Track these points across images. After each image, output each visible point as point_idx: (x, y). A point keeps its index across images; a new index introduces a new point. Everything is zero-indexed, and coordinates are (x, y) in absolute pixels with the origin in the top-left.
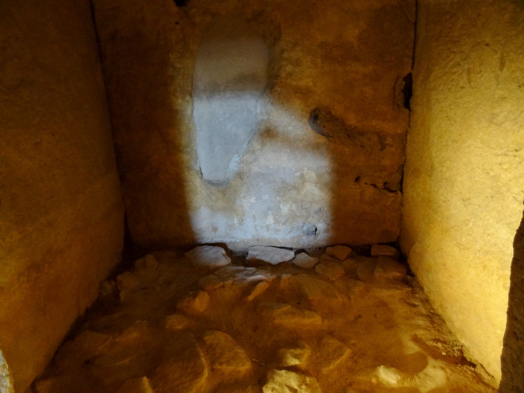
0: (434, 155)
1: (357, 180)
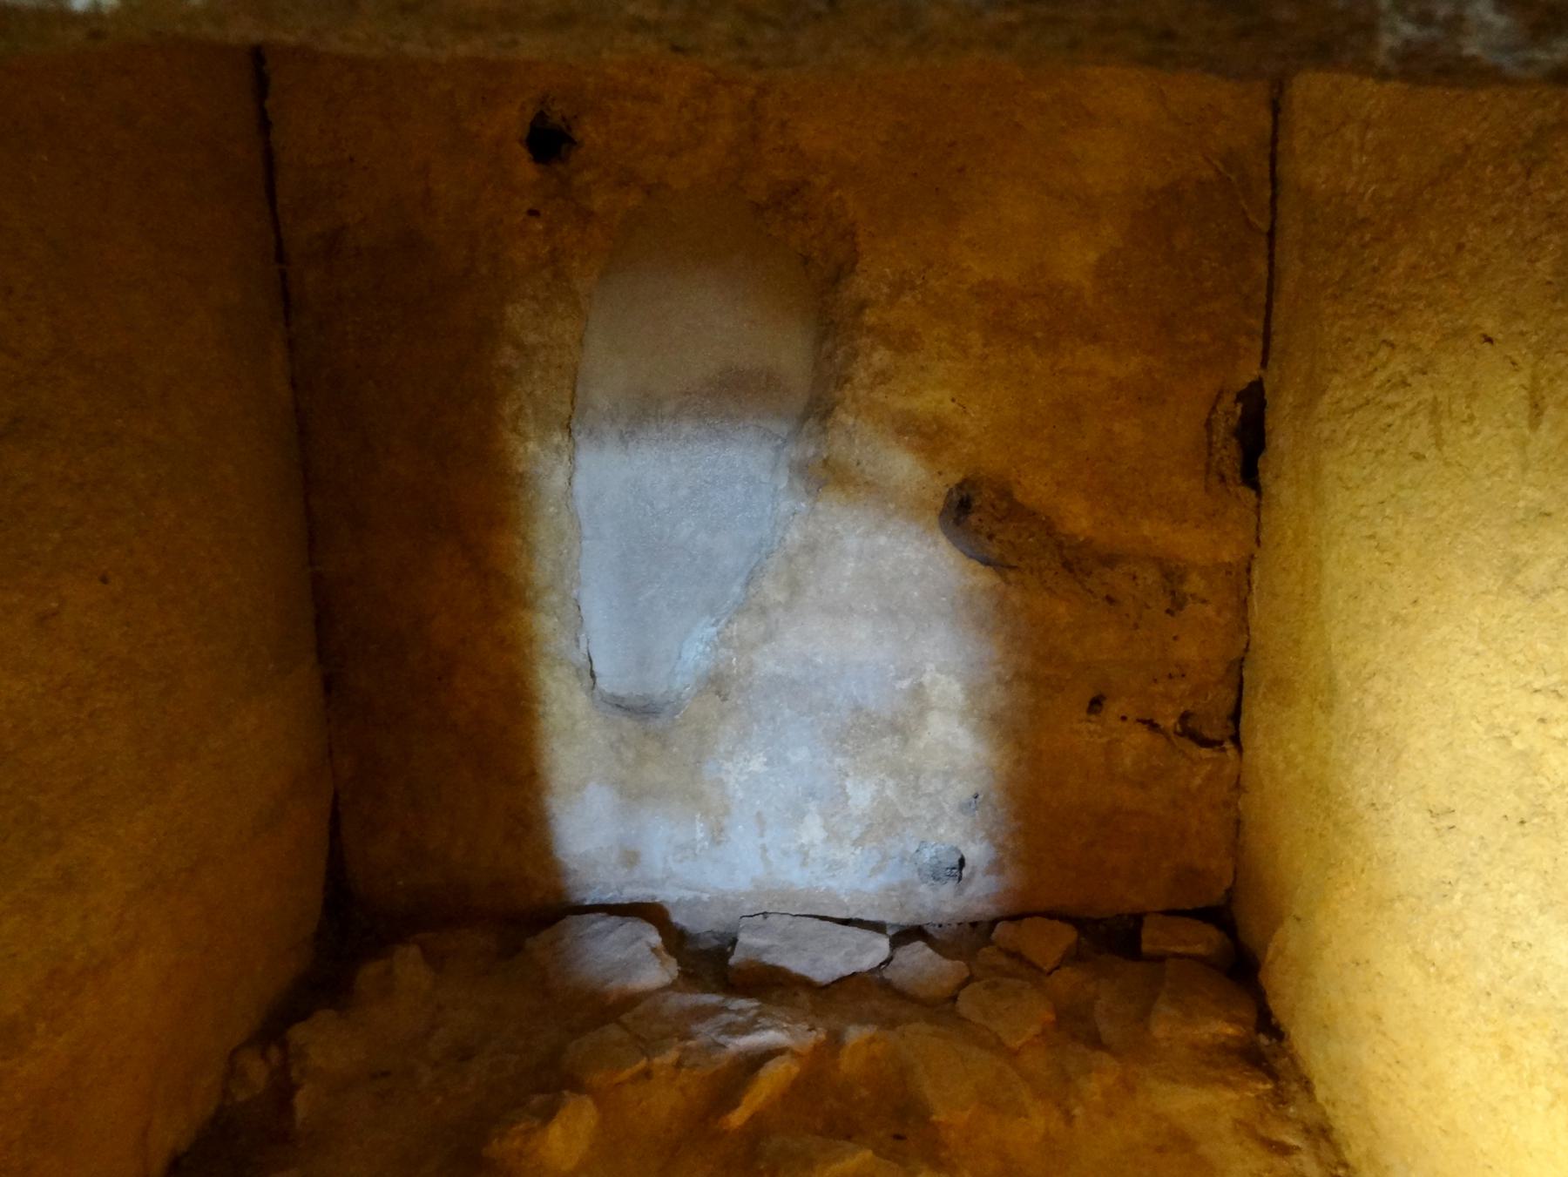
0: (1335, 648)
1: (1096, 704)
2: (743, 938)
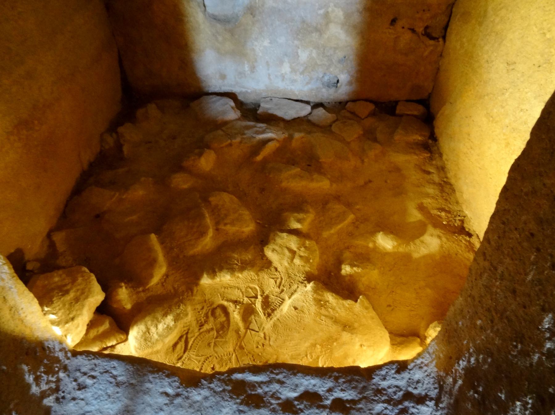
2: (262, 105)
